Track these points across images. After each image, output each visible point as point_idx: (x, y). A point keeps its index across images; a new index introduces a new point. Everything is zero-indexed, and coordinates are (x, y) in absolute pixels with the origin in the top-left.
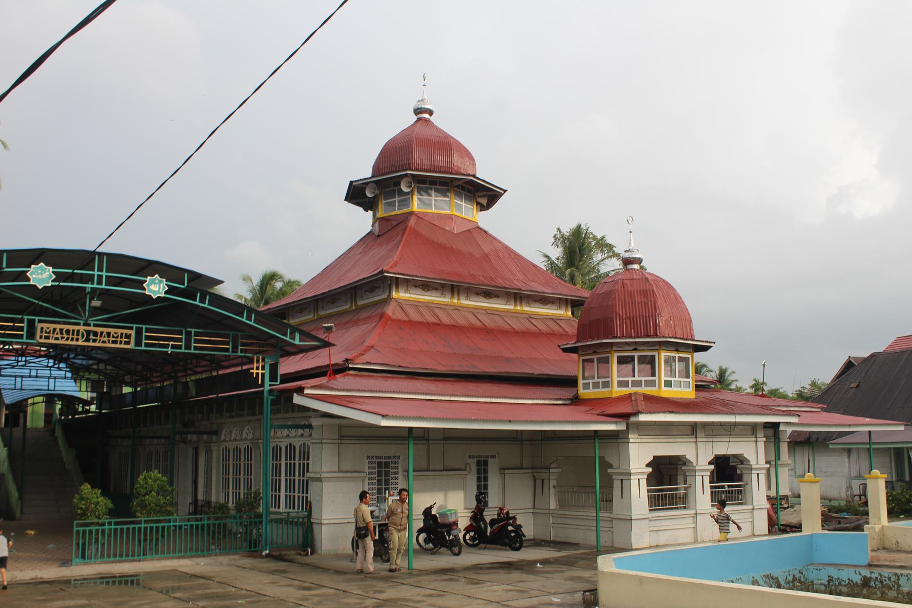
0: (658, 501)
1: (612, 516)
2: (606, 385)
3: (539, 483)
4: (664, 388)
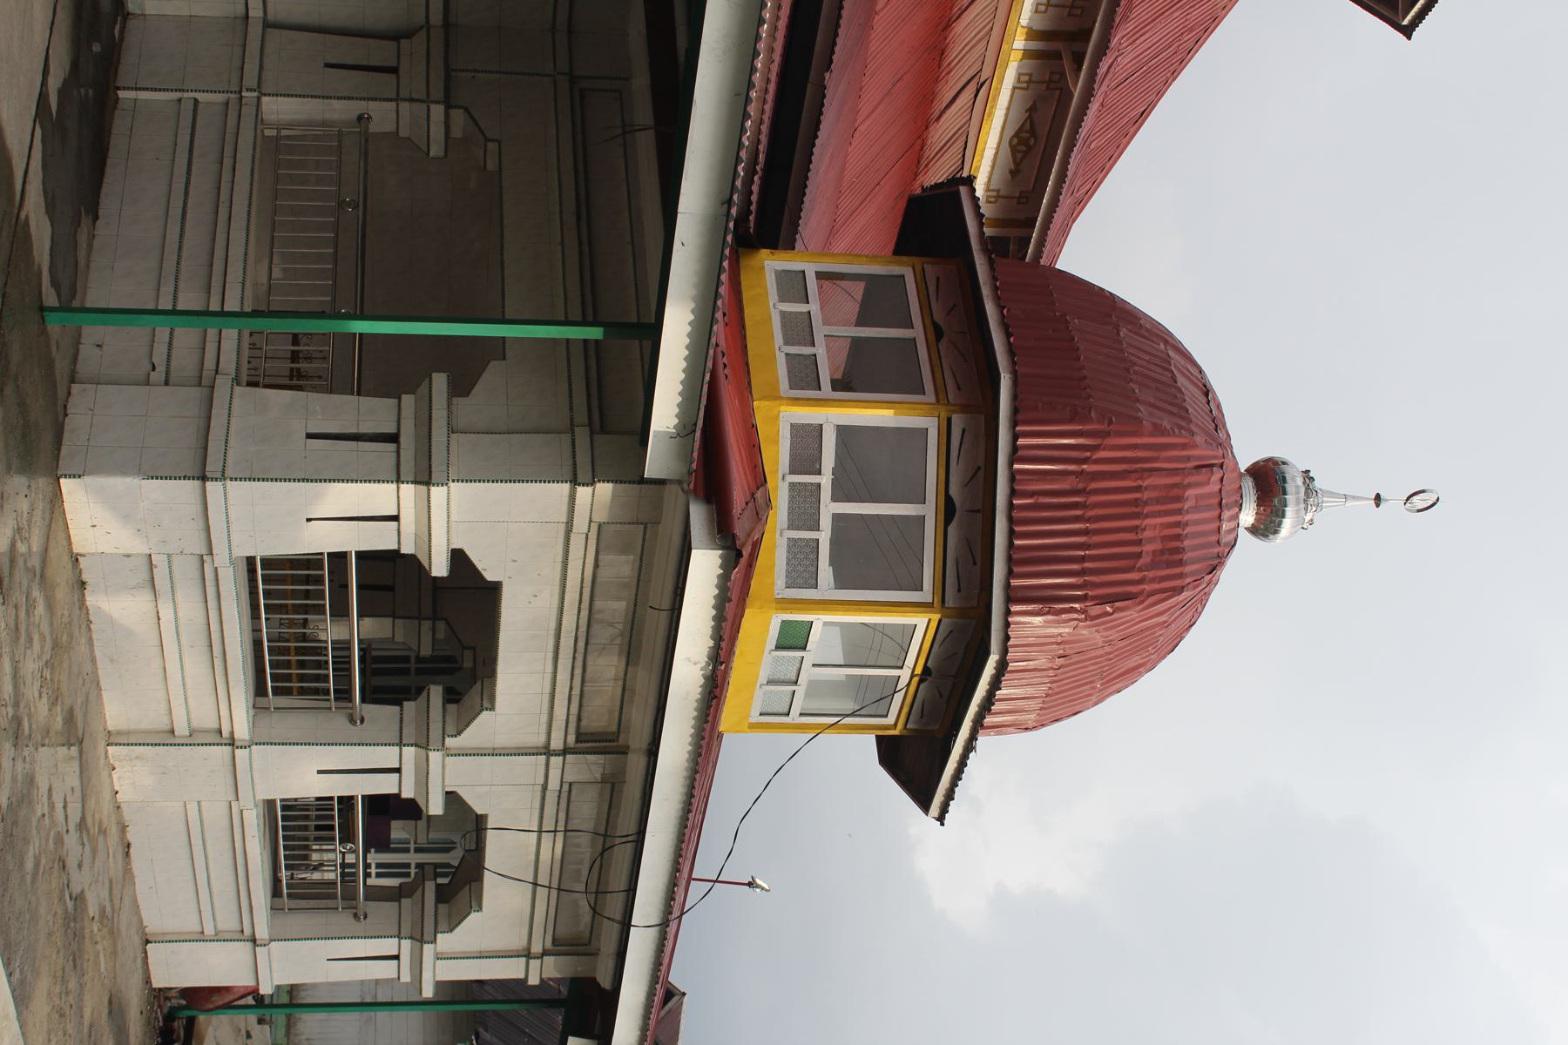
0: (287, 588)
1: (223, 385)
2: (804, 376)
3: (381, 53)
4: (776, 620)
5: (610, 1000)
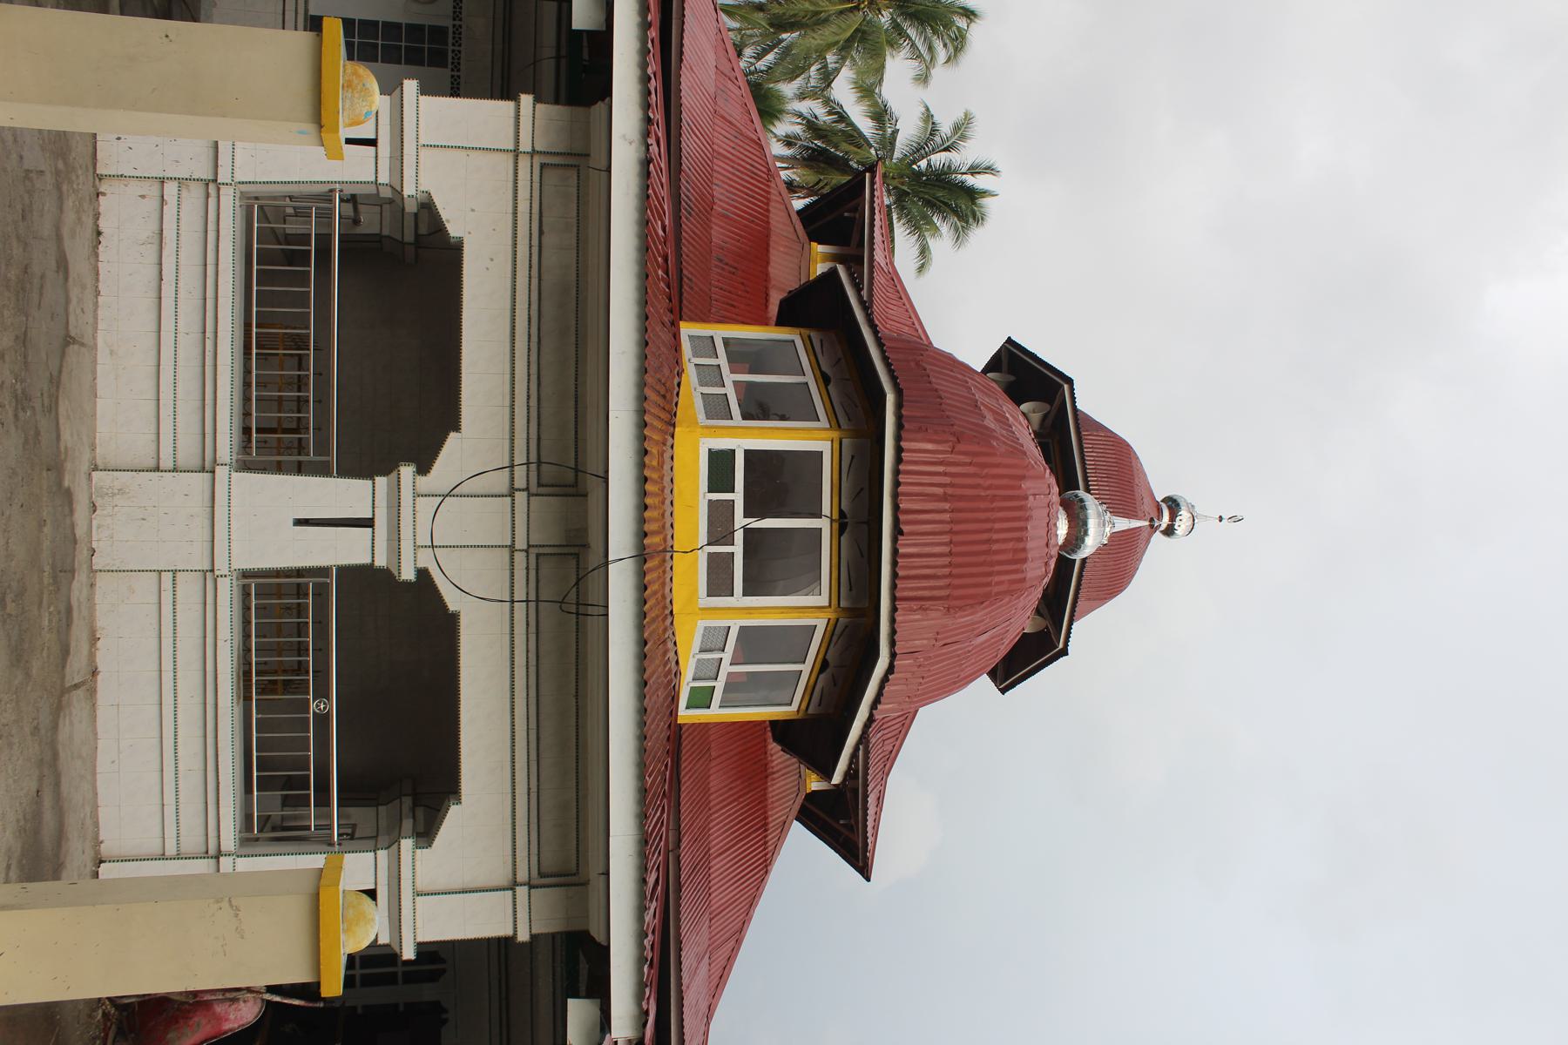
2: (716, 408)
5: (600, 955)
